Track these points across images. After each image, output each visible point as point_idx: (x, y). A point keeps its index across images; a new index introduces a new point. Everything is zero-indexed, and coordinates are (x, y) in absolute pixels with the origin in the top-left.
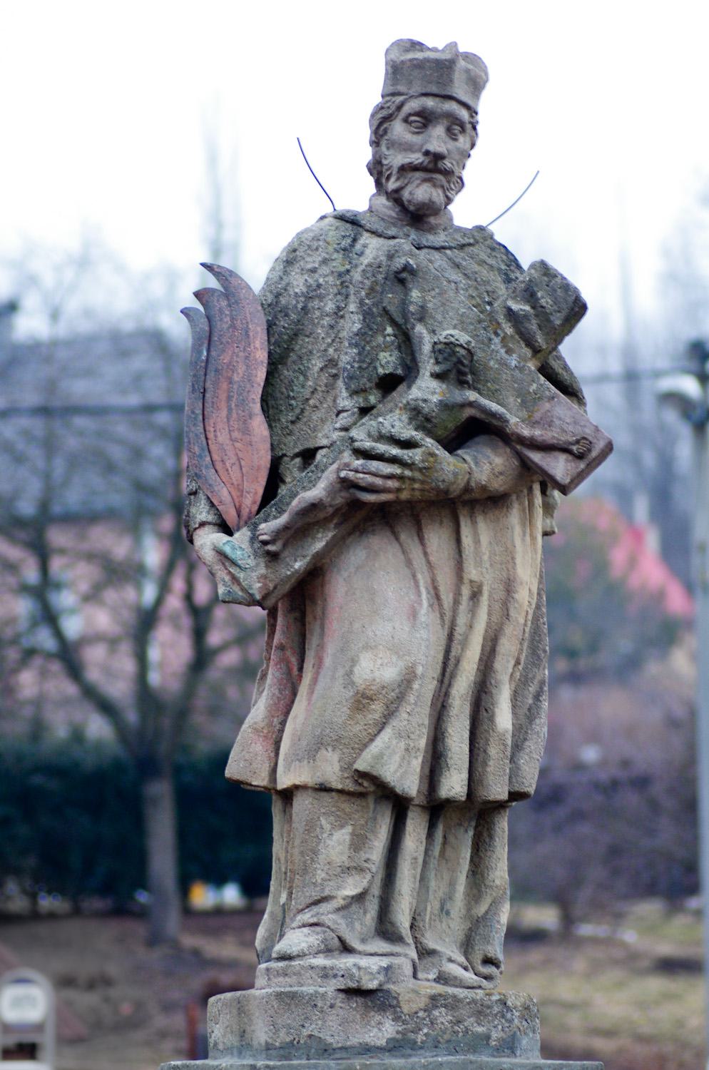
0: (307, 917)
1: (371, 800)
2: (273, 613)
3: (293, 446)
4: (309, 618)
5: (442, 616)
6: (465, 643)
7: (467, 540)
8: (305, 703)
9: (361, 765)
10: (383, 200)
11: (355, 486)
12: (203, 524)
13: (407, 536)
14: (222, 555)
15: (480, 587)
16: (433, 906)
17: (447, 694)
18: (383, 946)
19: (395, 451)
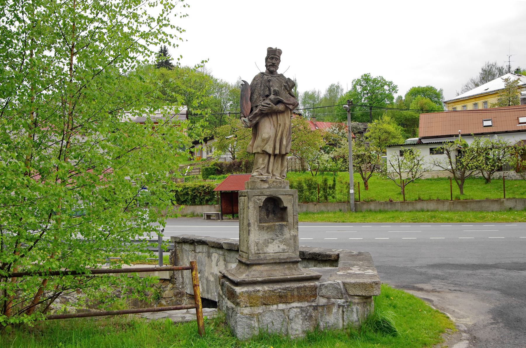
3: (254, 105)
19: (267, 105)
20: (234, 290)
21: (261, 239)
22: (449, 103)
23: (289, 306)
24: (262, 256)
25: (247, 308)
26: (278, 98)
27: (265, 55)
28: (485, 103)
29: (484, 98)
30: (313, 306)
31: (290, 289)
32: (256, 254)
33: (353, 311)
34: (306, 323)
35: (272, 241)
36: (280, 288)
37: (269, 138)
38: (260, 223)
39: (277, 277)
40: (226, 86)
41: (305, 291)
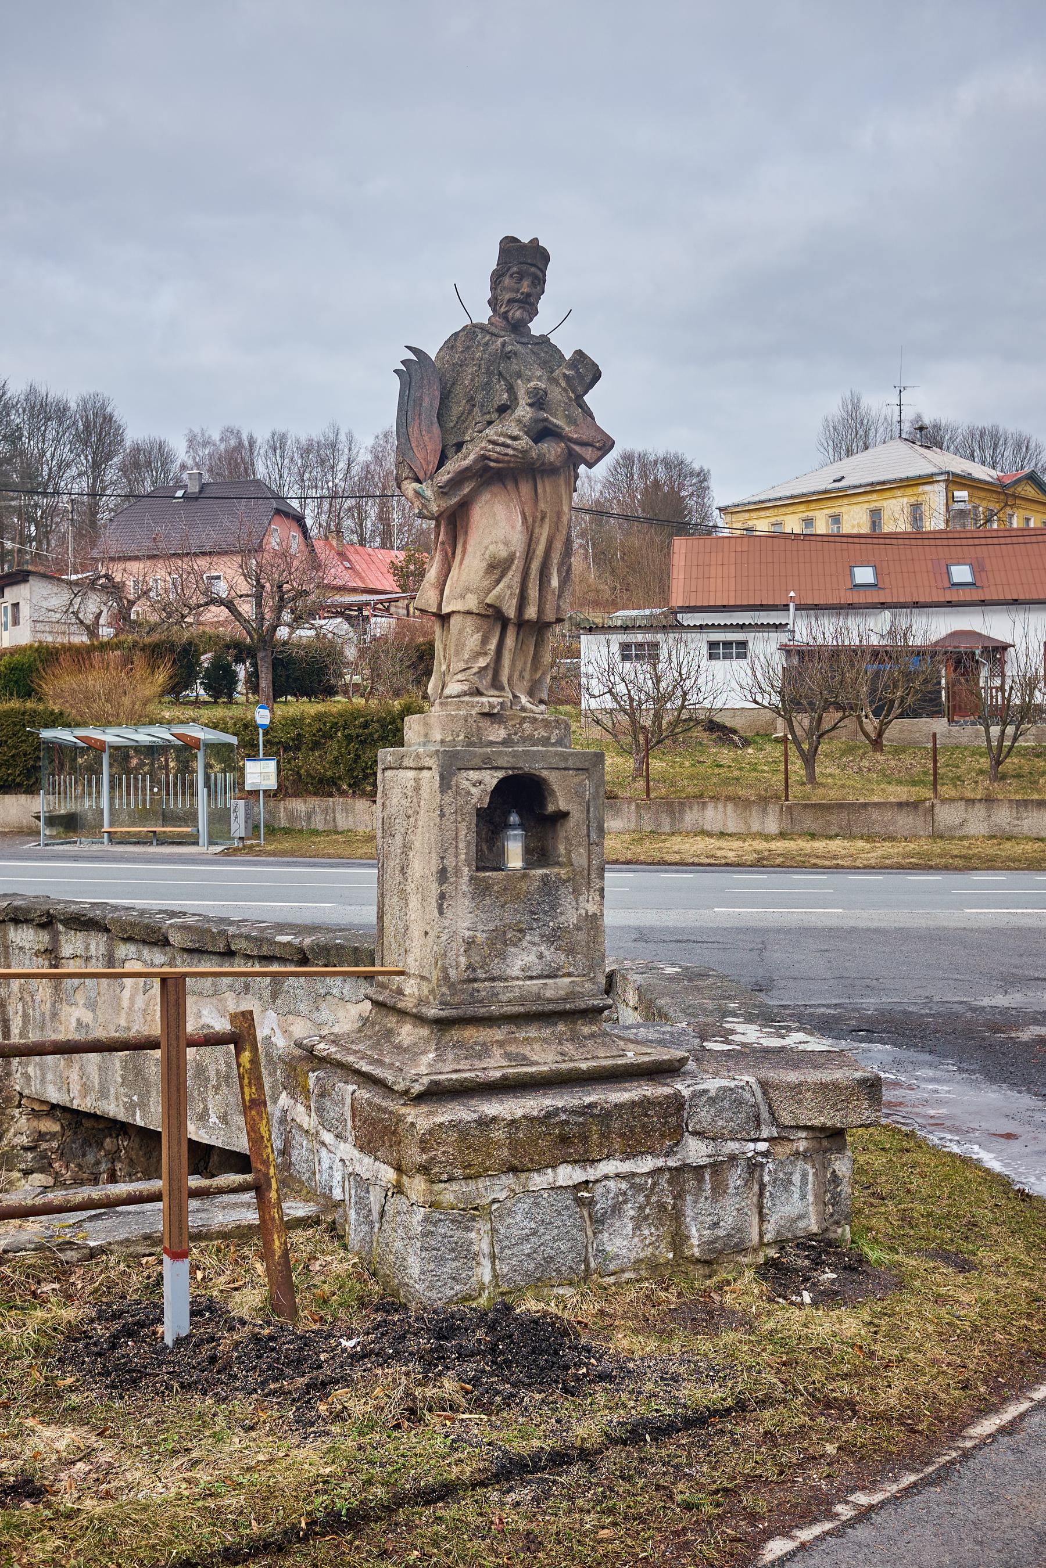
0: (460, 676)
1: (492, 618)
2: (438, 526)
3: (453, 440)
4: (459, 527)
5: (527, 528)
6: (538, 543)
7: (540, 490)
8: (457, 571)
9: (488, 601)
10: (497, 320)
11: (489, 458)
12: (406, 478)
13: (510, 486)
14: (418, 494)
15: (546, 513)
16: (516, 675)
17: (529, 568)
18: (496, 693)
19: (509, 442)
20: (400, 1119)
21: (480, 927)
22: (732, 513)
23: (592, 1173)
24: (483, 987)
25: (454, 1186)
26: (546, 420)
27: (491, 261)
28: (876, 515)
29: (830, 503)
30: (670, 1169)
31: (596, 1111)
32: (464, 981)
33: (790, 1182)
34: (646, 1232)
35: (520, 935)
36: (564, 1110)
37: (511, 558)
38: (478, 869)
39: (546, 1068)
40: (531, 320)
41: (647, 1115)
